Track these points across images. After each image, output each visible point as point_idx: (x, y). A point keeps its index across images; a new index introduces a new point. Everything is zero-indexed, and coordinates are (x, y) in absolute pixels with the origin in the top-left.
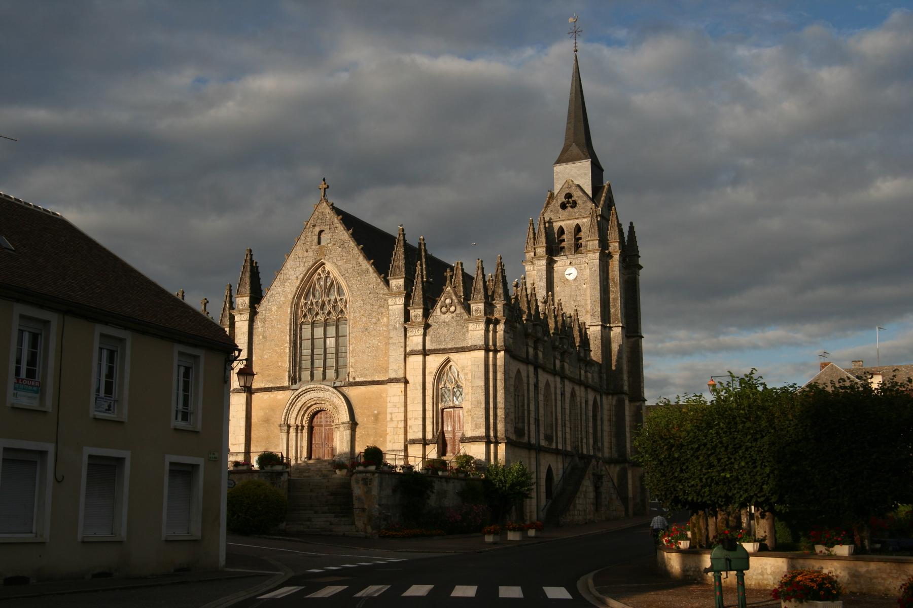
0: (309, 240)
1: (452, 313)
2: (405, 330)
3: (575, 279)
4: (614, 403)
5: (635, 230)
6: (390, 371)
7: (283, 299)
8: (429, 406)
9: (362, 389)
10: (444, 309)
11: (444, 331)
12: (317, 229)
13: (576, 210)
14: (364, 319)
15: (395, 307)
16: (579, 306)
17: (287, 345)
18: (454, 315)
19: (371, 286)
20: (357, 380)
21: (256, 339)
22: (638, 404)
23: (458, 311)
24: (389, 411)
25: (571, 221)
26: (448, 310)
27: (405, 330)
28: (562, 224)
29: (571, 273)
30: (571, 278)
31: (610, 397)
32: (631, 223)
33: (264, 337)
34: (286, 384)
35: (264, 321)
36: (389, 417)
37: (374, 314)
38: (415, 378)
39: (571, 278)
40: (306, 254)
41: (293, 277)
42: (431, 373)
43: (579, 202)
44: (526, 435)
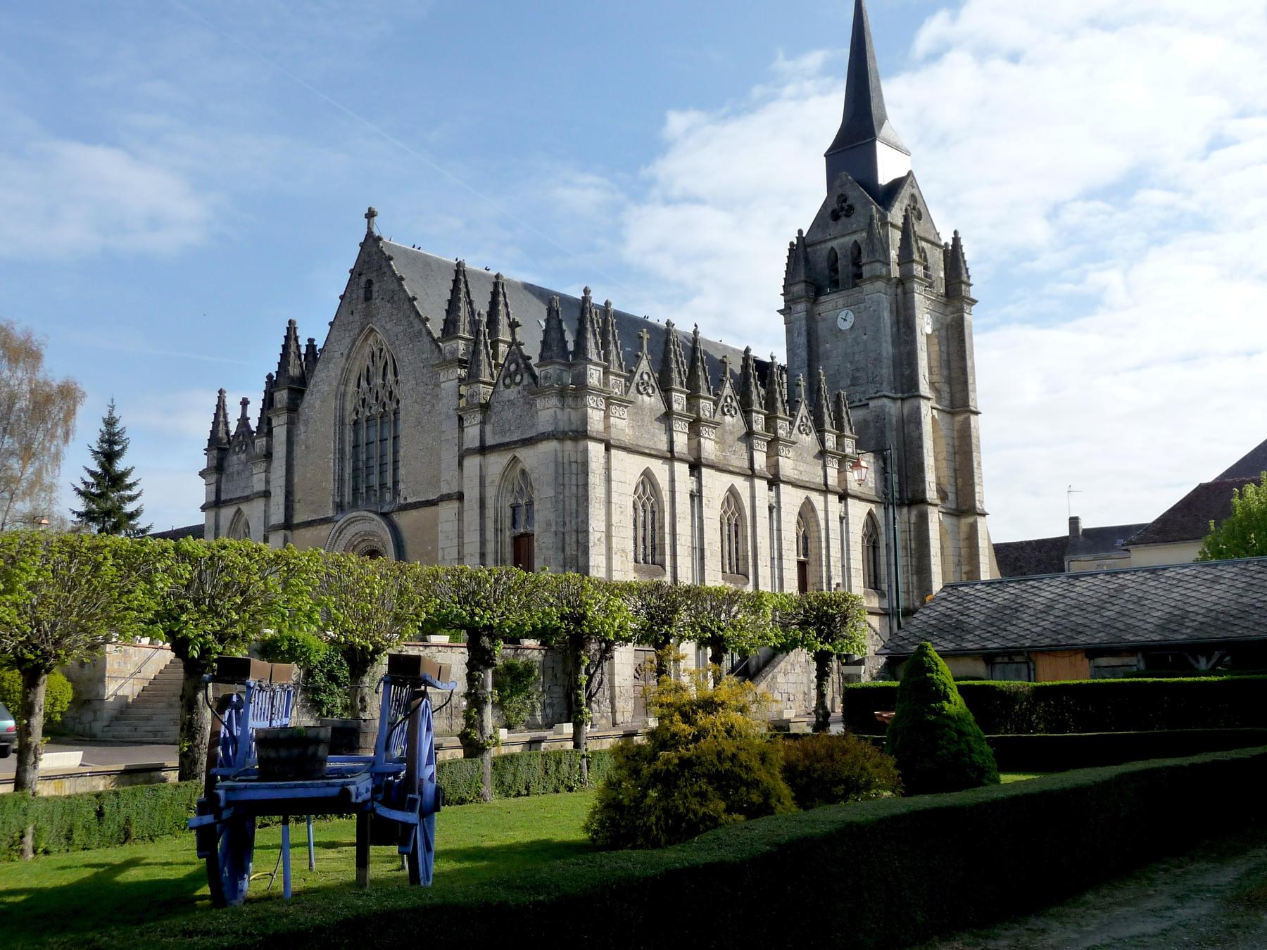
0: (354, 296)
1: (518, 384)
2: (461, 419)
3: (852, 327)
4: (913, 520)
5: (963, 242)
6: (443, 484)
7: (327, 388)
8: (490, 534)
9: (414, 513)
10: (508, 381)
11: (508, 414)
12: (364, 279)
13: (853, 219)
14: (417, 407)
15: (448, 384)
16: (857, 370)
17: (331, 456)
18: (520, 388)
19: (424, 356)
20: (409, 500)
21: (299, 450)
22: (971, 520)
23: (525, 382)
24: (441, 545)
25: (846, 239)
26: (513, 381)
27: (461, 419)
28: (834, 244)
29: (846, 320)
30: (845, 326)
31: (905, 510)
32: (956, 233)
33: (307, 447)
34: (330, 514)
35: (307, 422)
36: (440, 554)
37: (429, 398)
38: (471, 494)
39: (845, 326)
40: (351, 318)
41: (337, 354)
42: (493, 481)
43: (858, 207)
44: (668, 568)
